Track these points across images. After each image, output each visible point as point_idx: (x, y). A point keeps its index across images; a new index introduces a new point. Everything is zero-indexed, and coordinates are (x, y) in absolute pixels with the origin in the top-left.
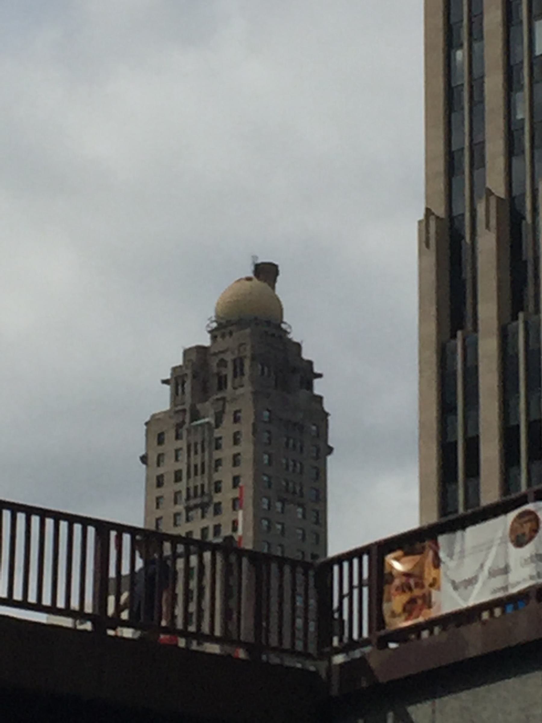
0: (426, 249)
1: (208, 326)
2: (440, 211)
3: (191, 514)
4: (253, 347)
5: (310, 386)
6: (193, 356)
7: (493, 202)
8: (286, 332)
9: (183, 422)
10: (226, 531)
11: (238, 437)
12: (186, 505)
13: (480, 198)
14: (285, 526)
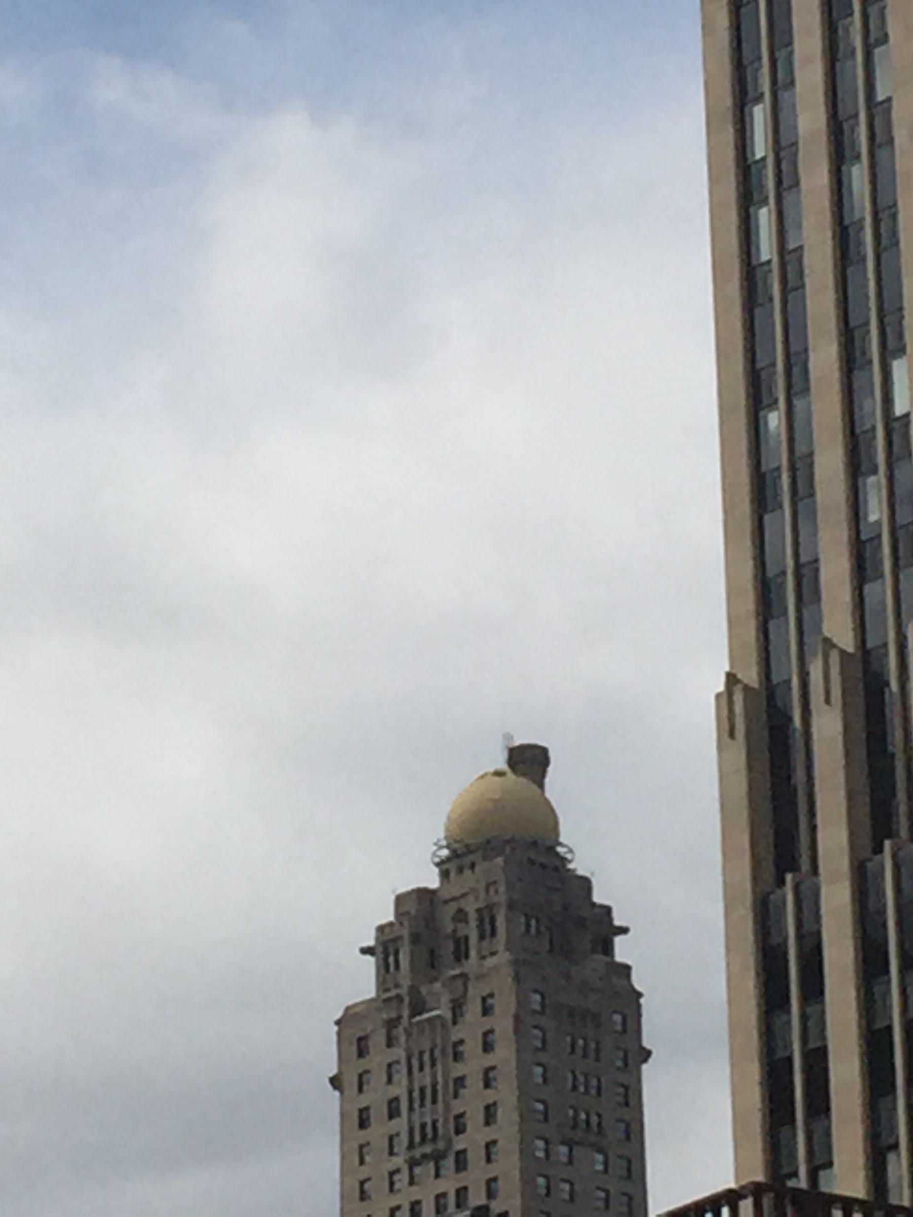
0: (728, 740)
1: (434, 854)
2: (751, 676)
3: (417, 1170)
4: (510, 886)
5: (608, 948)
6: (411, 907)
7: (834, 658)
8: (564, 860)
9: (400, 1017)
10: (477, 1198)
11: (461, 1048)
12: (407, 1157)
13: (815, 655)
14: (576, 1187)
